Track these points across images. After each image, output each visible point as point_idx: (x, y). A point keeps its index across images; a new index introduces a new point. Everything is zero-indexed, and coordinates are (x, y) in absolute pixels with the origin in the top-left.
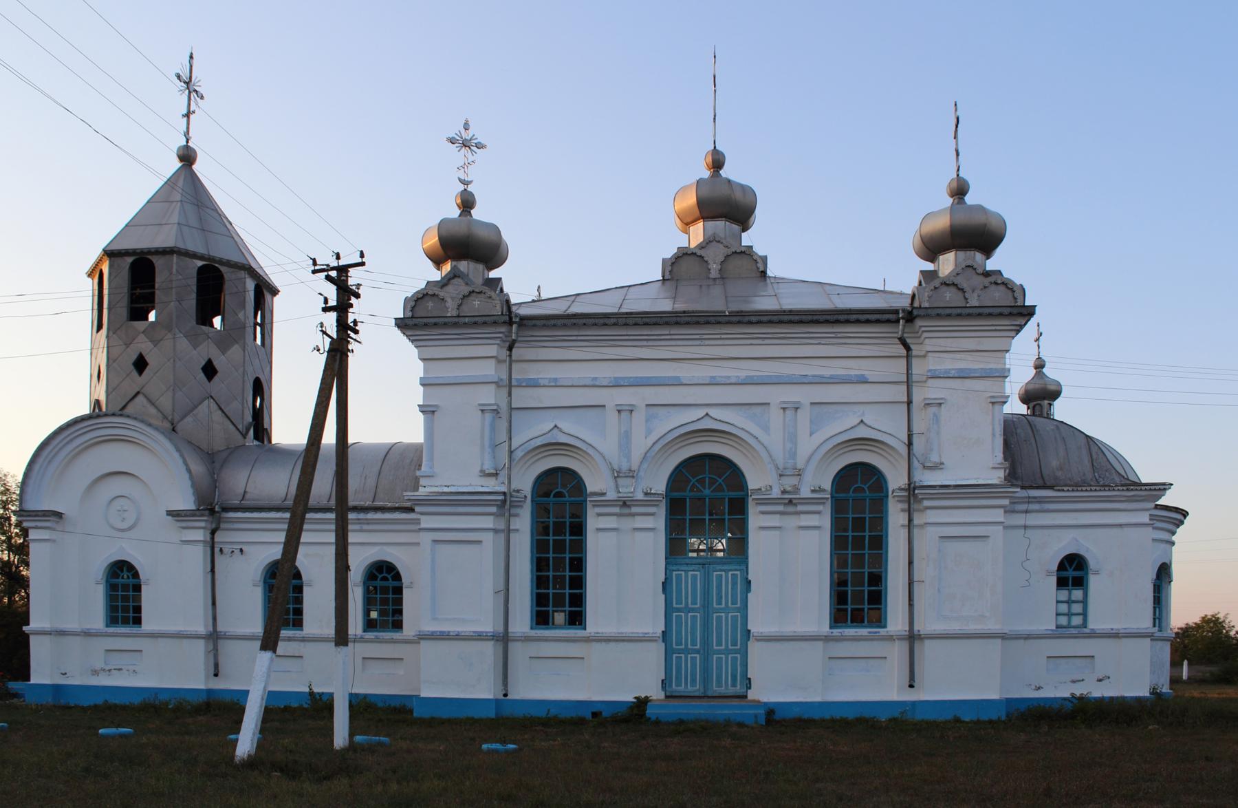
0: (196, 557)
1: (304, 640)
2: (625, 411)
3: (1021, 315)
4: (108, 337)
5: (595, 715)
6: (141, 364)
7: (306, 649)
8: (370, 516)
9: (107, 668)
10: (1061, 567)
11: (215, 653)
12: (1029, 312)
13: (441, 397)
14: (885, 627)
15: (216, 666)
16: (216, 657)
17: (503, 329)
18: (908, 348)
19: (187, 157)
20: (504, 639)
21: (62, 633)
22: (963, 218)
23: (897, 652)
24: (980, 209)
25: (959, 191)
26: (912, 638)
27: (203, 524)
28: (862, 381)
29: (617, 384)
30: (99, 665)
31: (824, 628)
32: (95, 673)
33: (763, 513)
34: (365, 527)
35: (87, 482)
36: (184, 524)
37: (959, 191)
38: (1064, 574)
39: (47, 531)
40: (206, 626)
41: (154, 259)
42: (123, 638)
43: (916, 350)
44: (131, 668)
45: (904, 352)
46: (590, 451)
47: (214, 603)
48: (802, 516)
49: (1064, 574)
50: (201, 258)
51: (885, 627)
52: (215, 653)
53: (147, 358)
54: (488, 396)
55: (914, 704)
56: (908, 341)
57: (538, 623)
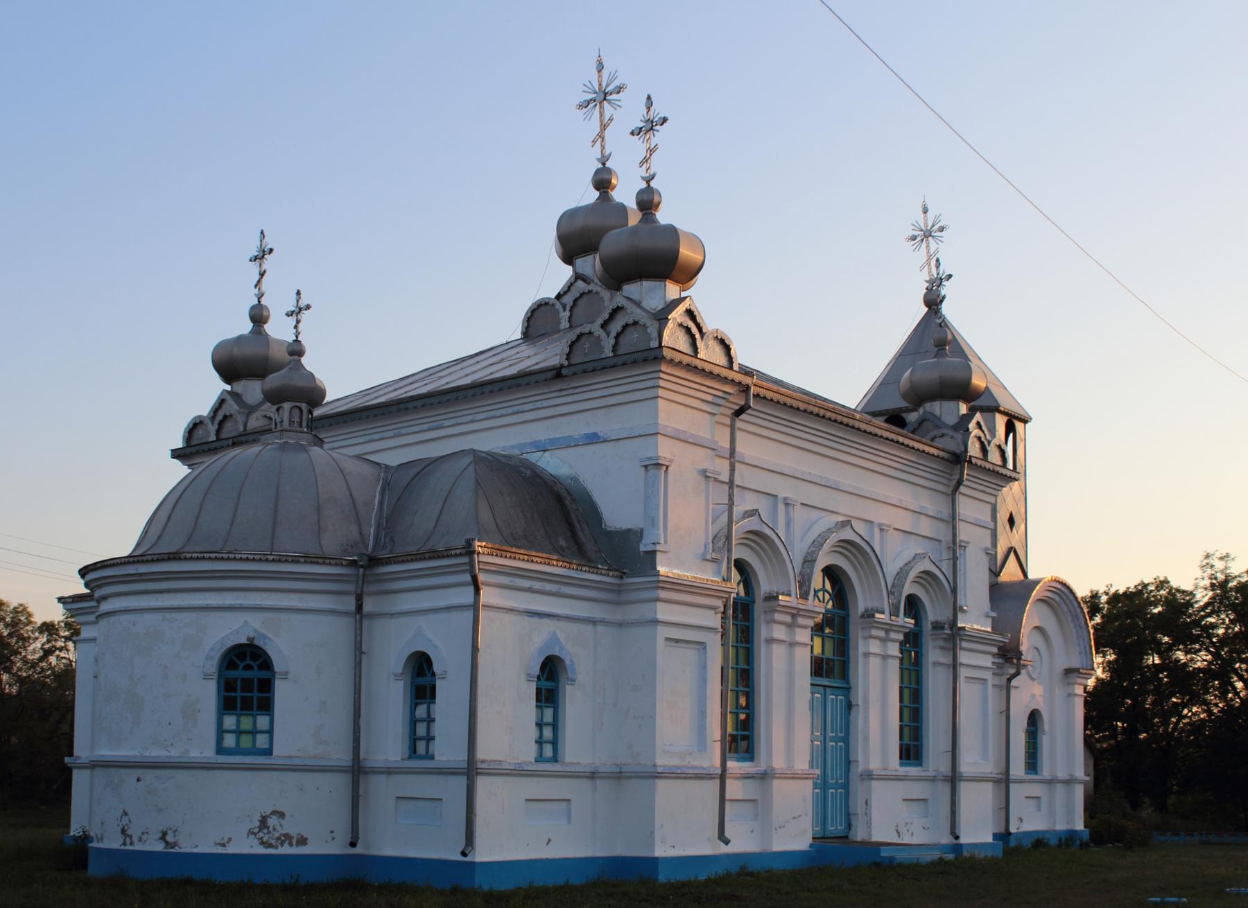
38: (232, 674)
49: (264, 674)
55: (728, 856)
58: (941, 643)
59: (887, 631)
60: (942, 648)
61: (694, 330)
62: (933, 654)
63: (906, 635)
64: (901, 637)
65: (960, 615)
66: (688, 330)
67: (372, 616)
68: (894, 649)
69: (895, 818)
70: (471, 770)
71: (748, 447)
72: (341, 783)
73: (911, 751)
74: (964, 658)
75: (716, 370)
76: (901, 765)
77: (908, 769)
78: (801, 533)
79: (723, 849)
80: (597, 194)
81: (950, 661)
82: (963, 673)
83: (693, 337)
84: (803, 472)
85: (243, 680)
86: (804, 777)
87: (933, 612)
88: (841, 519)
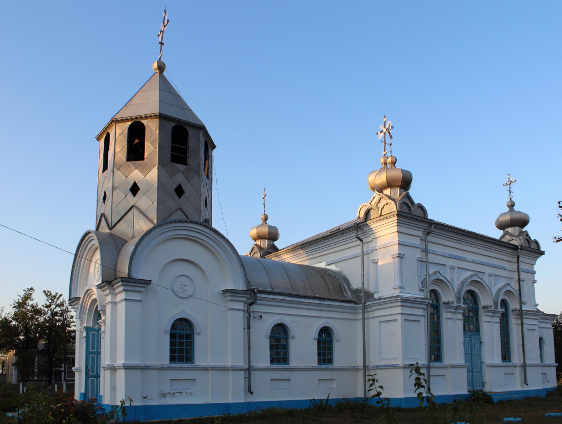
0: (240, 317)
1: (333, 370)
2: (452, 268)
3: (539, 253)
4: (158, 168)
5: (455, 401)
6: (180, 191)
7: (293, 376)
8: (326, 302)
9: (172, 392)
10: (173, 327)
11: (248, 379)
12: (542, 253)
13: (407, 252)
14: (511, 362)
15: (250, 387)
16: (250, 381)
17: (427, 226)
18: (361, 240)
19: (161, 68)
20: (249, 370)
21: (146, 368)
22: (515, 216)
23: (518, 372)
24: (519, 212)
25: (512, 205)
26: (524, 366)
27: (245, 299)
28: (504, 269)
29: (451, 257)
30: (166, 391)
31: (166, 361)
32: (164, 395)
33: (488, 316)
34: (320, 308)
35: (165, 264)
36: (234, 298)
37: (512, 205)
38: (174, 331)
39: (139, 294)
40: (245, 363)
41: (145, 122)
42: (182, 372)
43: (364, 241)
44: (188, 391)
45: (359, 242)
46: (449, 284)
47: (249, 349)
48: (376, 311)
49: (174, 331)
50: (127, 120)
51: (511, 362)
52: (248, 379)
53: (184, 188)
54: (418, 254)
55: (527, 391)
56: (361, 238)
57: (286, 362)
58: (516, 316)
59: (456, 309)
60: (516, 318)
61: (410, 204)
62: (514, 322)
63: (502, 315)
64: (500, 315)
65: (523, 305)
66: (407, 204)
67: (368, 318)
68: (498, 320)
69: (500, 382)
70: (524, 366)
71: (431, 247)
72: (241, 375)
73: (506, 355)
74: (525, 321)
75: (406, 215)
76: (503, 362)
77: (174, 365)
78: (457, 279)
79: (526, 388)
80: (508, 209)
81: (520, 322)
82: (525, 327)
83: (409, 207)
84: (444, 253)
85: (179, 334)
86: (553, 366)
87: (513, 305)
88: (473, 273)
